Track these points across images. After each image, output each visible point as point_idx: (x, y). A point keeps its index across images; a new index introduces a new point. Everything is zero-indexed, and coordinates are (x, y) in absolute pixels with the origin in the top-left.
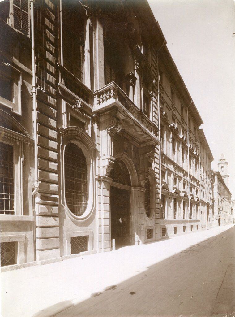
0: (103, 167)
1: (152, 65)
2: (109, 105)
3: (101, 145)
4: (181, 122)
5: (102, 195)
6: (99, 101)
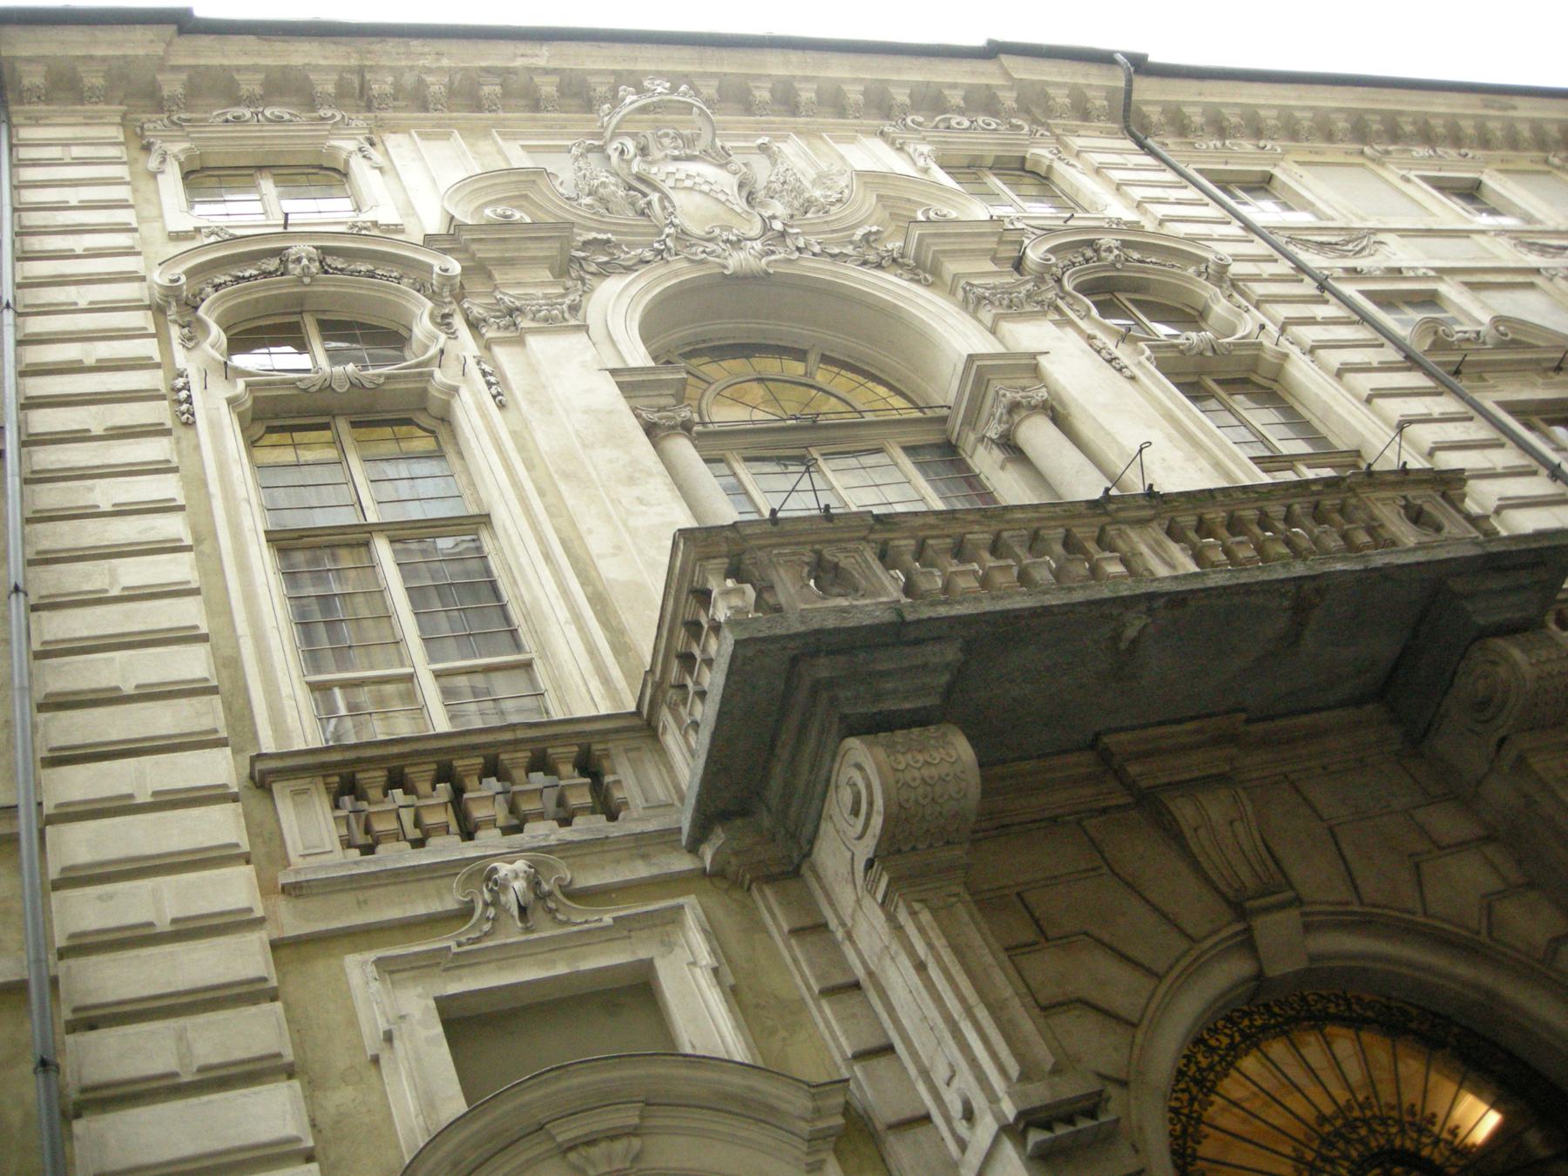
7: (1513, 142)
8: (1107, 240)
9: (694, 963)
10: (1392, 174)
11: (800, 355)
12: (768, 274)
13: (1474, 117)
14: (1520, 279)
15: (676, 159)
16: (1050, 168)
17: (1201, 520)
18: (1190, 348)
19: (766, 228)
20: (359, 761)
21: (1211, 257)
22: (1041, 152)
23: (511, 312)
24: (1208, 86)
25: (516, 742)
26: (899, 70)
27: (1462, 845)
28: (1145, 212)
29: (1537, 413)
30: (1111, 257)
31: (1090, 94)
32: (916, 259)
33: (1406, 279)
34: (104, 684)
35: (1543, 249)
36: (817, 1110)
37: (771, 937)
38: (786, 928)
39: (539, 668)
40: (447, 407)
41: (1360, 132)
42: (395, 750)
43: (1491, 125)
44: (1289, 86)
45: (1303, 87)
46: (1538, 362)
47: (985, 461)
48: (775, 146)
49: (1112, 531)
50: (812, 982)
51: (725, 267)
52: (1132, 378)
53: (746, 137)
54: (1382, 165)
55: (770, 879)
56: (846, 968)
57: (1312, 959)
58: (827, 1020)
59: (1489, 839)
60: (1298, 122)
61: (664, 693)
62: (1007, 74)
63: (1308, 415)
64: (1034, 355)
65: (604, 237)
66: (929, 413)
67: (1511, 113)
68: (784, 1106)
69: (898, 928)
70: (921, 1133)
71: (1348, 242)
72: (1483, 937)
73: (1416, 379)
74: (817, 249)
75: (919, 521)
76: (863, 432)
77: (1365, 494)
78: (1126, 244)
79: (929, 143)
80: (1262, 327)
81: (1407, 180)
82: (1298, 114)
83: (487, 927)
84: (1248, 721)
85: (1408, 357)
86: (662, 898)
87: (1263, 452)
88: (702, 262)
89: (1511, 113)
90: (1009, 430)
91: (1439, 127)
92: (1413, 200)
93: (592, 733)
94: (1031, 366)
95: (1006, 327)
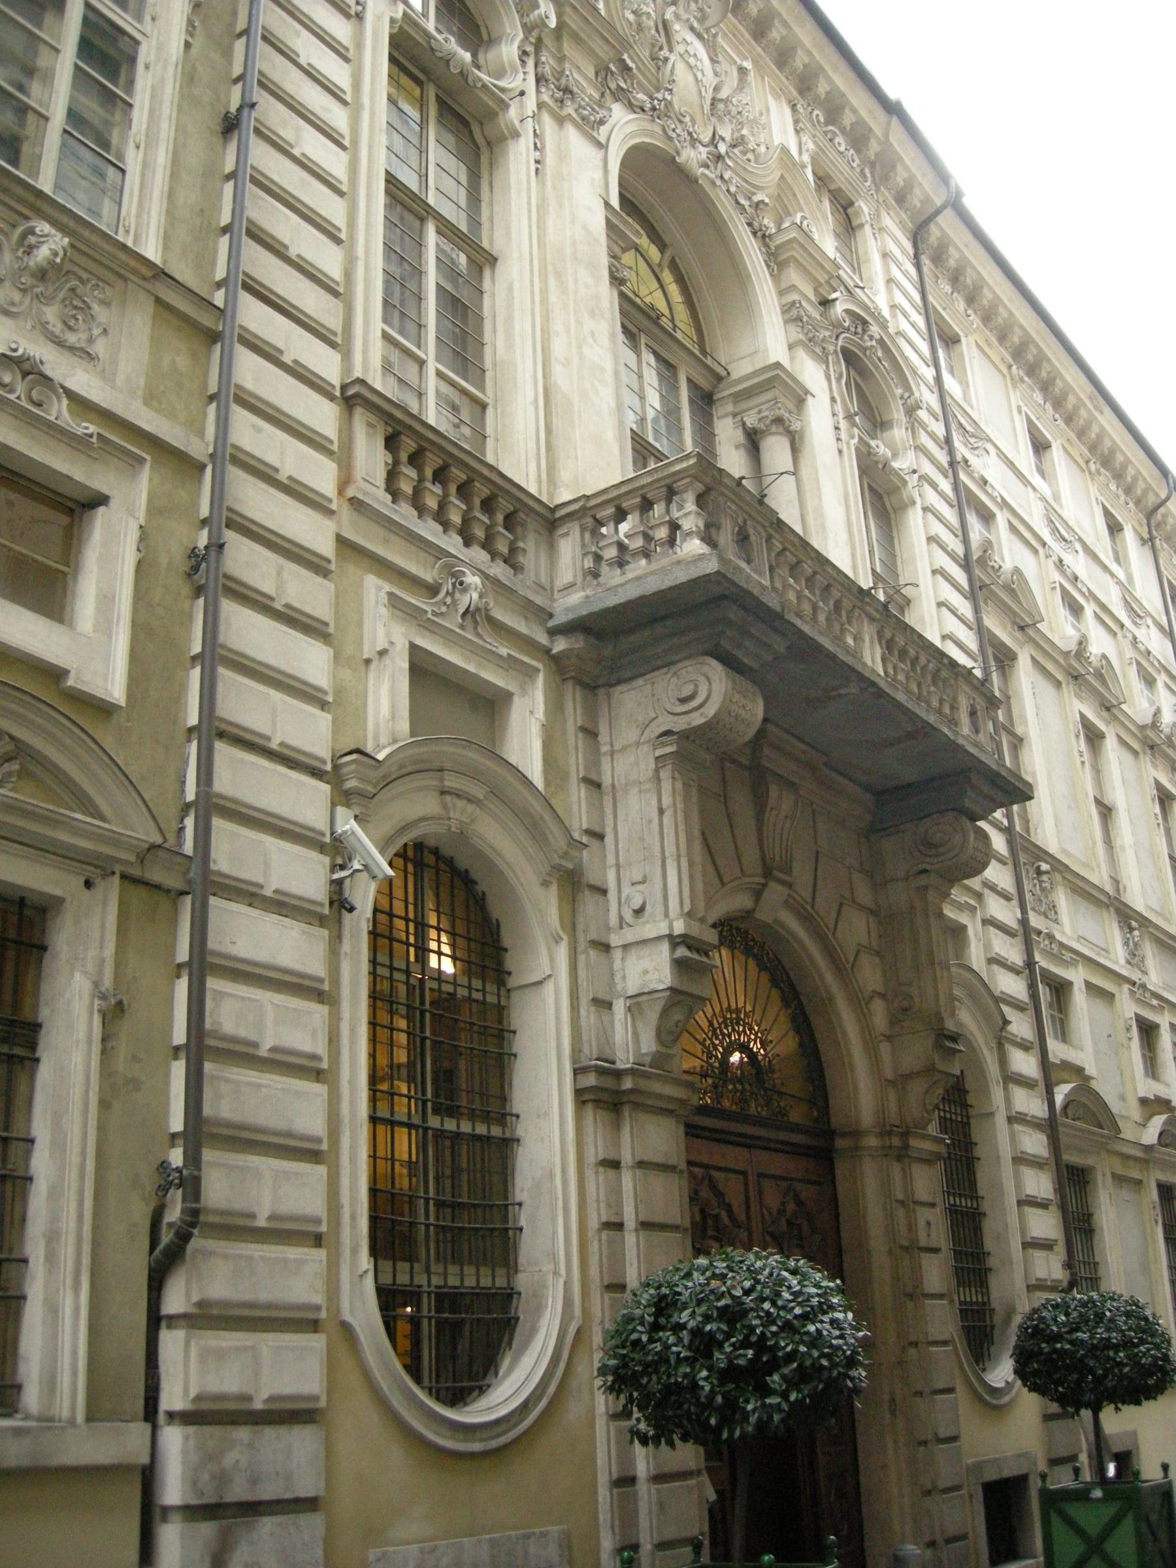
0: (636, 1003)
1: (893, 307)
2: (670, 588)
3: (609, 839)
4: (1123, 616)
5: (630, 1222)
6: (598, 558)
7: (1081, 434)
8: (874, 329)
9: (531, 712)
10: (1015, 399)
11: (662, 247)
12: (696, 181)
13: (1079, 399)
14: (1034, 542)
15: (692, 29)
16: (861, 226)
17: (892, 639)
18: (876, 454)
19: (714, 140)
20: (410, 427)
21: (917, 394)
22: (864, 208)
23: (567, 90)
24: (974, 244)
25: (490, 481)
26: (836, 69)
27: (861, 907)
28: (894, 316)
29: (993, 646)
30: (869, 344)
31: (917, 191)
32: (777, 248)
33: (986, 492)
34: (280, 237)
35: (1055, 530)
36: (566, 853)
37: (565, 721)
38: (579, 723)
39: (490, 412)
40: (502, 139)
41: (1018, 353)
42: (431, 436)
43: (1083, 412)
44: (1013, 288)
45: (1018, 294)
46: (1015, 614)
47: (727, 434)
48: (751, 77)
49: (857, 612)
50: (581, 768)
51: (678, 153)
52: (840, 452)
53: (739, 53)
54: (1015, 387)
55: (579, 682)
56: (599, 773)
57: (775, 921)
58: (578, 794)
59: (872, 912)
60: (996, 314)
61: (584, 516)
62: (886, 134)
63: (898, 552)
64: (807, 392)
65: (631, 64)
66: (709, 361)
67: (1097, 414)
68: (552, 840)
69: (658, 779)
70: (600, 898)
71: (973, 436)
72: (848, 967)
73: (960, 577)
74: (733, 189)
75: (791, 537)
76: (675, 347)
77: (961, 680)
78: (881, 342)
79: (815, 143)
80: (522, 93)
81: (1020, 412)
82: (1001, 310)
83: (444, 609)
84: (825, 764)
85: (967, 556)
86: (534, 658)
87: (410, 180)
88: (670, 139)
89: (1097, 414)
90: (763, 432)
91: (969, 279)
92: (1014, 429)
93: (526, 505)
94: (800, 397)
95: (801, 353)
